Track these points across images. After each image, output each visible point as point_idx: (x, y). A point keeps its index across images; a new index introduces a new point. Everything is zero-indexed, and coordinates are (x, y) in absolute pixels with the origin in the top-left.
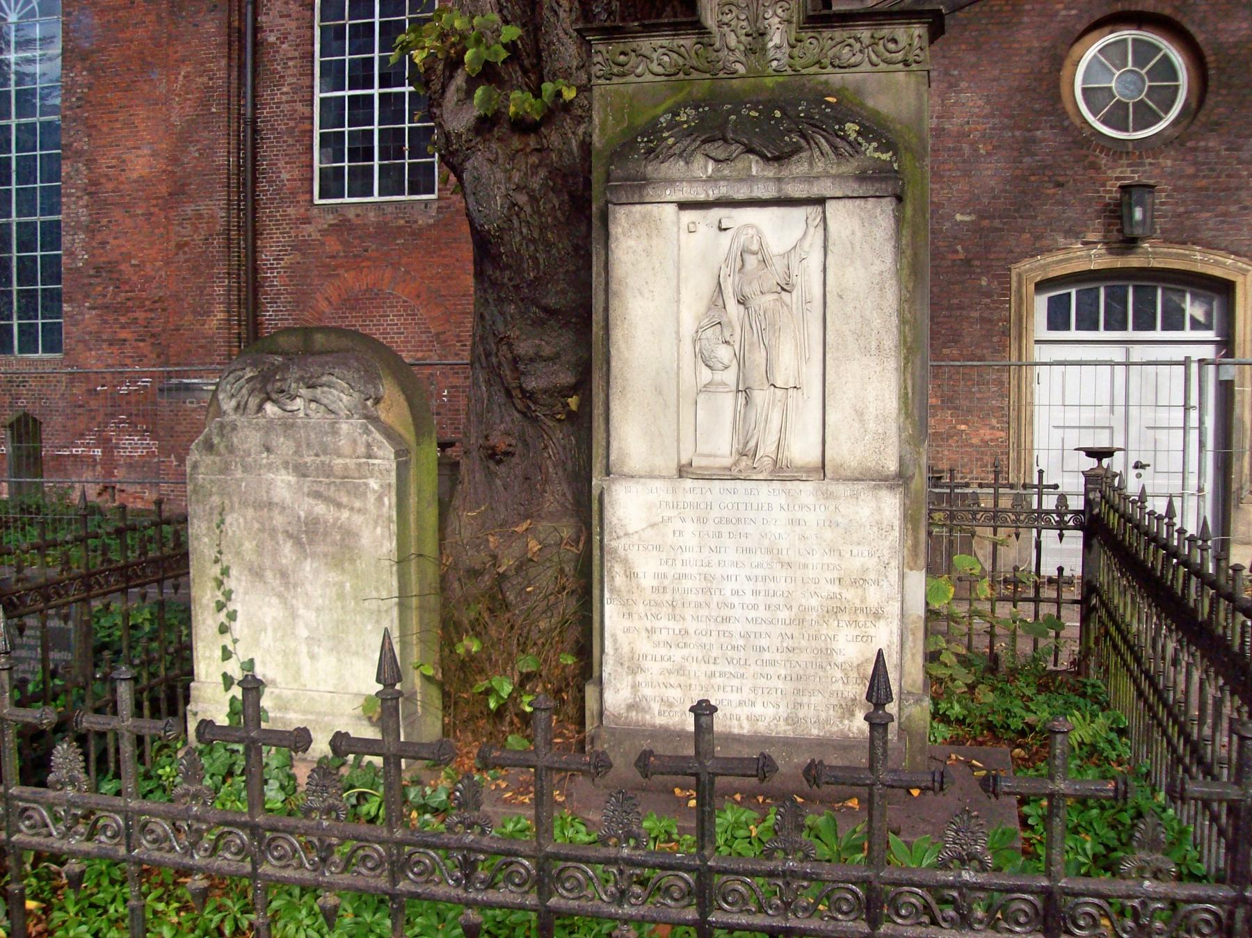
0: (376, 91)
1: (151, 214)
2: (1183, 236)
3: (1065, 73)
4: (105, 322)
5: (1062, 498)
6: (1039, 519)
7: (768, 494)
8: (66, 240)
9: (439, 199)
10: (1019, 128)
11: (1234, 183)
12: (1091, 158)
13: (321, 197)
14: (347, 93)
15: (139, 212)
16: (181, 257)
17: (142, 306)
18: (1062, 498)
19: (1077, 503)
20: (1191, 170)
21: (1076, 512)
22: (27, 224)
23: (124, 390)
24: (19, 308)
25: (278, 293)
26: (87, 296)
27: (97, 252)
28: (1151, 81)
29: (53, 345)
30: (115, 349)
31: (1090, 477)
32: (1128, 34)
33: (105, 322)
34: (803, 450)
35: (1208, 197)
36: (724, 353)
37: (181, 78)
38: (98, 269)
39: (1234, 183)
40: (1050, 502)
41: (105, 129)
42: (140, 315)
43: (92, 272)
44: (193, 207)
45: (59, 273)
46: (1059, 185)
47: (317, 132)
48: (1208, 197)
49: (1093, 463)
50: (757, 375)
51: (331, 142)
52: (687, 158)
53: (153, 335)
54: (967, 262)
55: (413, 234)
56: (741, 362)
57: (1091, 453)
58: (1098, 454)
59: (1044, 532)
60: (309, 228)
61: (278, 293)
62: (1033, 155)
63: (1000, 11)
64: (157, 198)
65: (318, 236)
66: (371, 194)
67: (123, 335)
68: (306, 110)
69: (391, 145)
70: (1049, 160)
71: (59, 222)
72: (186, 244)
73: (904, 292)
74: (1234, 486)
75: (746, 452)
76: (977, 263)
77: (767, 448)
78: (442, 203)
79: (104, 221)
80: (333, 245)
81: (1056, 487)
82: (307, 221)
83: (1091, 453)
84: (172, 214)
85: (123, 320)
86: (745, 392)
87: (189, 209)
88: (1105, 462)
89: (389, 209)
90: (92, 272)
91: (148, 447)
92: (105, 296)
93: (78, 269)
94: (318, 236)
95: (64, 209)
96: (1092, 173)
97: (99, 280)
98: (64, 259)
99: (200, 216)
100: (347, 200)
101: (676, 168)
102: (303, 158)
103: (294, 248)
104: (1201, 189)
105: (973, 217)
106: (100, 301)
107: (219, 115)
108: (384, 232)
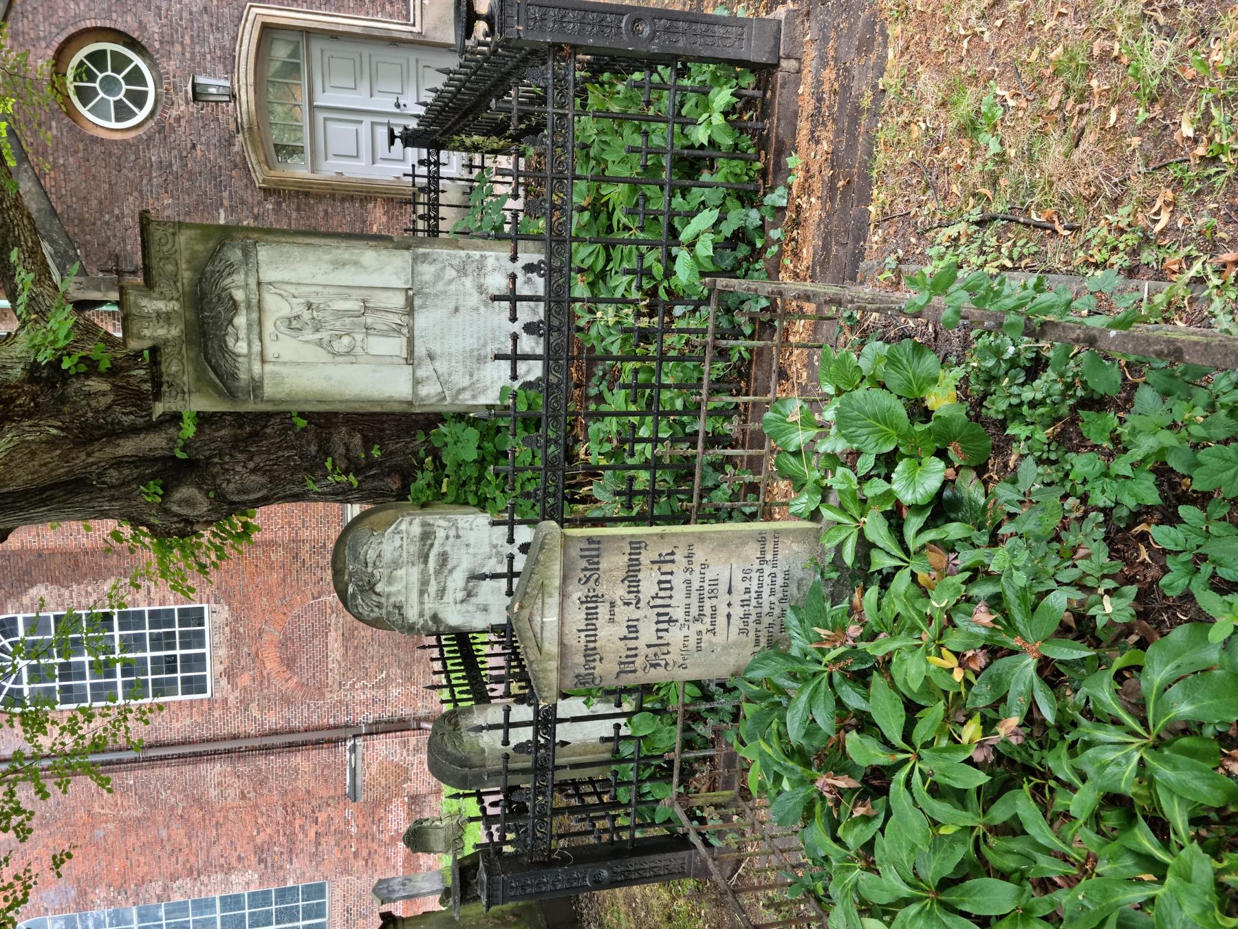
1: (217, 823)
4: (302, 850)
5: (421, 162)
6: (434, 178)
8: (236, 890)
9: (208, 602)
10: (150, 172)
12: (172, 121)
13: (204, 691)
15: (214, 833)
18: (421, 162)
19: (424, 153)
20: (178, 48)
21: (429, 153)
23: (354, 830)
24: (291, 921)
26: (281, 867)
27: (246, 864)
28: (119, 73)
29: (319, 890)
30: (323, 840)
31: (406, 143)
33: (302, 850)
35: (199, 36)
37: (103, 812)
40: (423, 170)
41: (146, 869)
42: (297, 823)
43: (262, 866)
44: (212, 790)
45: (263, 892)
46: (194, 146)
48: (199, 36)
49: (398, 141)
51: (161, 688)
53: (313, 811)
55: (236, 621)
57: (392, 142)
58: (392, 138)
59: (540, 363)
60: (231, 698)
62: (171, 165)
63: (55, 179)
64: (204, 820)
65: (237, 693)
66: (204, 654)
67: (312, 835)
70: (175, 152)
71: (221, 898)
72: (242, 793)
74: (410, 37)
76: (256, 211)
78: (212, 600)
79: (222, 861)
80: (244, 680)
81: (413, 166)
82: (225, 700)
83: (392, 142)
84: (217, 807)
85: (301, 836)
87: (213, 793)
88: (397, 133)
89: (217, 639)
90: (262, 866)
92: (282, 853)
94: (237, 693)
95: (211, 895)
96: (183, 122)
97: (269, 859)
98: (252, 890)
99: (220, 784)
100: (208, 673)
104: (192, 41)
105: (222, 211)
106: (285, 856)
108: (235, 641)
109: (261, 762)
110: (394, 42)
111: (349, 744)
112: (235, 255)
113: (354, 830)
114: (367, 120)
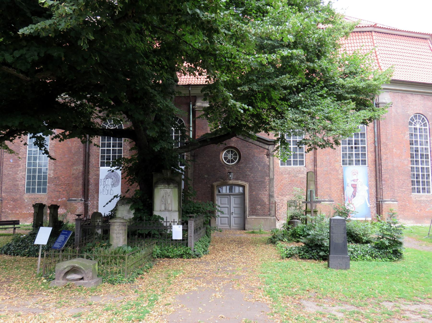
0: (111, 148)
2: (237, 179)
3: (221, 155)
7: (167, 212)
11: (245, 171)
14: (106, 148)
16: (73, 176)
17: (64, 185)
22: (40, 169)
23: (59, 200)
25: (92, 183)
32: (231, 149)
34: (170, 209)
36: (164, 201)
38: (55, 178)
39: (245, 171)
46: (220, 171)
47: (100, 155)
50: (166, 203)
52: (161, 185)
53: (66, 190)
54: (206, 183)
56: (165, 201)
61: (92, 183)
68: (98, 151)
69: (114, 158)
73: (70, 254)
75: (165, 209)
77: (167, 209)
85: (60, 187)
86: (165, 204)
91: (64, 211)
93: (51, 178)
99: (77, 169)
101: (160, 186)
102: (98, 159)
103: (95, 175)
107: (82, 151)
109: (81, 178)
110: (244, 212)
111: (83, 199)
112: (176, 185)
113: (59, 200)
114: (229, 206)
